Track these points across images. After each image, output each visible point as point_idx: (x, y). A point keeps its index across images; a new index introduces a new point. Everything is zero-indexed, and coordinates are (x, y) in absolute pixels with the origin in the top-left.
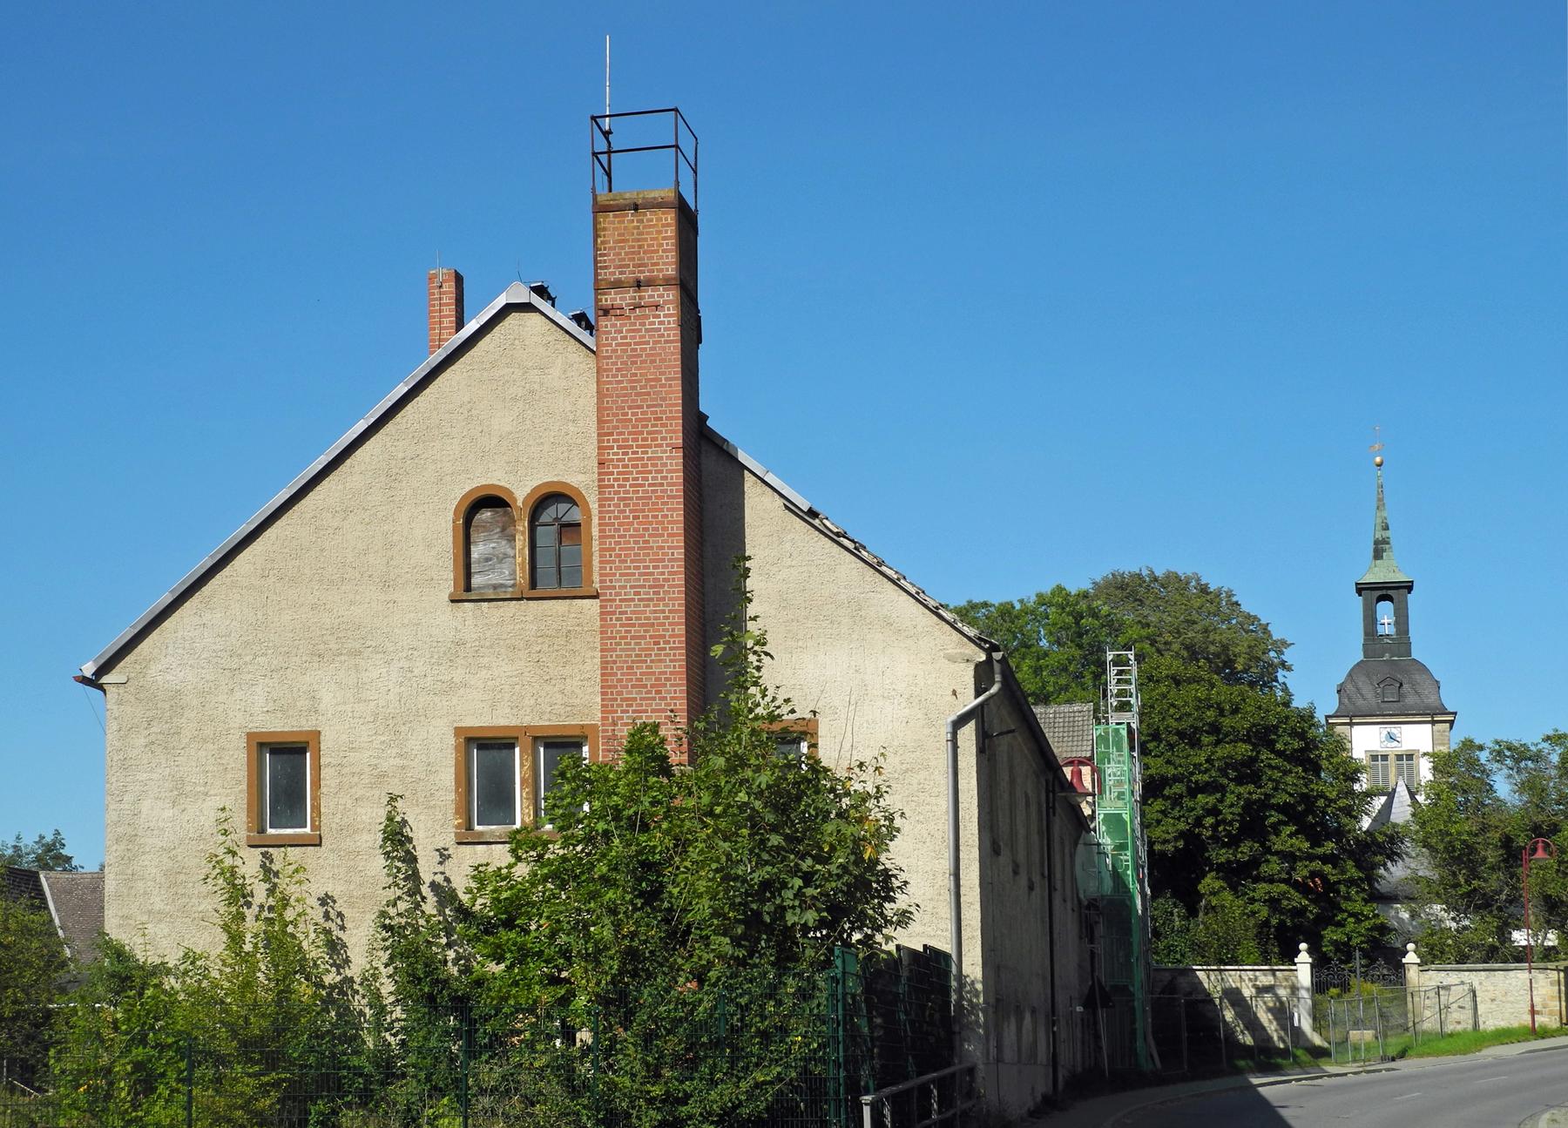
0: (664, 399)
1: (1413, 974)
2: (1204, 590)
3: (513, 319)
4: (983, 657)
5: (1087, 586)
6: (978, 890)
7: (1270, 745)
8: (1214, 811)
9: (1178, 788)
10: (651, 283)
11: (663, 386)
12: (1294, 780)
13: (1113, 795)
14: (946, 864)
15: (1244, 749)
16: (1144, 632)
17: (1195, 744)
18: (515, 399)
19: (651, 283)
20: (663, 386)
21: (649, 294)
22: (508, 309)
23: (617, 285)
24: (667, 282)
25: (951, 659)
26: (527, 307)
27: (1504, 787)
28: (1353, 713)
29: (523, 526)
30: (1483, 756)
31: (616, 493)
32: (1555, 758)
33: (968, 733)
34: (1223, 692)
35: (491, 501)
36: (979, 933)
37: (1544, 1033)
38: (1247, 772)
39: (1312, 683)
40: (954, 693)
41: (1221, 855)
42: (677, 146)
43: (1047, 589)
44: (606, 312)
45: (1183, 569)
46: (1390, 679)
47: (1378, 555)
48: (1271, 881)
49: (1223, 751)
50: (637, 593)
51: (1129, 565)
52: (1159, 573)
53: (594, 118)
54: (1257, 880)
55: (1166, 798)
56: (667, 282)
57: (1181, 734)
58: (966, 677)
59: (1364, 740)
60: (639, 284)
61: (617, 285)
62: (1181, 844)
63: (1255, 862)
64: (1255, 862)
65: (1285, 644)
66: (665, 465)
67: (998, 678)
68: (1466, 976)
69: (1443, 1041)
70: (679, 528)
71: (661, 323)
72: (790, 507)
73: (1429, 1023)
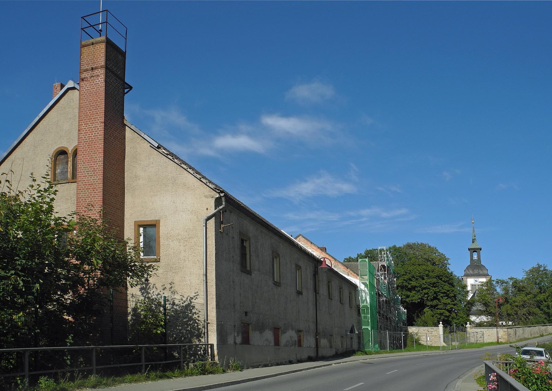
0: (99, 107)
1: (468, 329)
2: (430, 247)
3: (70, 91)
4: (218, 196)
5: (401, 245)
6: (215, 281)
7: (441, 279)
8: (427, 294)
9: (419, 289)
10: (96, 68)
11: (99, 102)
12: (447, 287)
13: (484, 318)
14: (203, 271)
15: (435, 280)
16: (414, 256)
17: (423, 279)
18: (70, 119)
19: (96, 68)
20: (99, 102)
21: (96, 72)
22: (69, 89)
23: (86, 70)
24: (101, 67)
25: (206, 197)
26: (74, 88)
27: (499, 290)
28: (468, 276)
29: (70, 159)
30: (494, 283)
31: (83, 140)
32: (511, 283)
33: (212, 222)
34: (431, 267)
35: (62, 152)
36: (215, 297)
37: (502, 343)
38: (434, 285)
39: (457, 267)
40: (207, 209)
41: (429, 303)
42: (107, 22)
43: (391, 246)
44: (83, 80)
45: (425, 242)
46: (476, 268)
47: (473, 242)
48: (441, 309)
49: (429, 281)
50: (88, 174)
51: (412, 241)
52: (420, 243)
53: (82, 18)
54: (438, 309)
55: (416, 291)
56: (101, 67)
57: (420, 276)
58: (212, 202)
59: (470, 282)
60: (92, 69)
61: (86, 70)
62: (419, 300)
63: (437, 305)
64: (437, 305)
65: (448, 259)
66: (98, 129)
67: (224, 203)
68: (482, 330)
69: (471, 345)
70: (101, 150)
71: (99, 81)
72: (152, 146)
73: (472, 340)
